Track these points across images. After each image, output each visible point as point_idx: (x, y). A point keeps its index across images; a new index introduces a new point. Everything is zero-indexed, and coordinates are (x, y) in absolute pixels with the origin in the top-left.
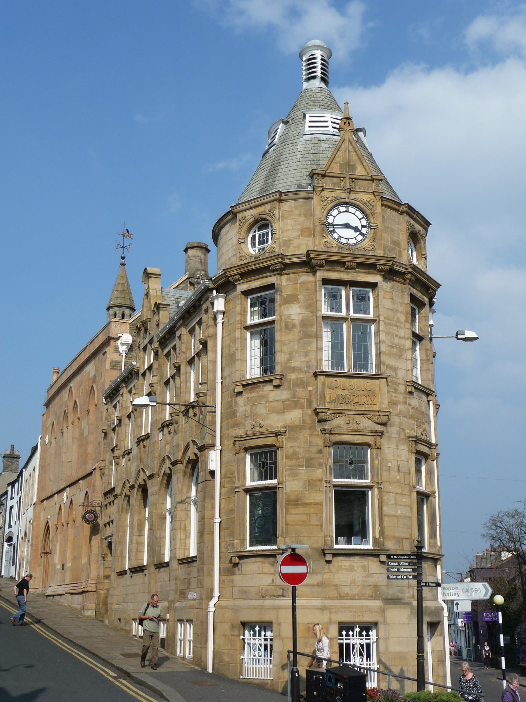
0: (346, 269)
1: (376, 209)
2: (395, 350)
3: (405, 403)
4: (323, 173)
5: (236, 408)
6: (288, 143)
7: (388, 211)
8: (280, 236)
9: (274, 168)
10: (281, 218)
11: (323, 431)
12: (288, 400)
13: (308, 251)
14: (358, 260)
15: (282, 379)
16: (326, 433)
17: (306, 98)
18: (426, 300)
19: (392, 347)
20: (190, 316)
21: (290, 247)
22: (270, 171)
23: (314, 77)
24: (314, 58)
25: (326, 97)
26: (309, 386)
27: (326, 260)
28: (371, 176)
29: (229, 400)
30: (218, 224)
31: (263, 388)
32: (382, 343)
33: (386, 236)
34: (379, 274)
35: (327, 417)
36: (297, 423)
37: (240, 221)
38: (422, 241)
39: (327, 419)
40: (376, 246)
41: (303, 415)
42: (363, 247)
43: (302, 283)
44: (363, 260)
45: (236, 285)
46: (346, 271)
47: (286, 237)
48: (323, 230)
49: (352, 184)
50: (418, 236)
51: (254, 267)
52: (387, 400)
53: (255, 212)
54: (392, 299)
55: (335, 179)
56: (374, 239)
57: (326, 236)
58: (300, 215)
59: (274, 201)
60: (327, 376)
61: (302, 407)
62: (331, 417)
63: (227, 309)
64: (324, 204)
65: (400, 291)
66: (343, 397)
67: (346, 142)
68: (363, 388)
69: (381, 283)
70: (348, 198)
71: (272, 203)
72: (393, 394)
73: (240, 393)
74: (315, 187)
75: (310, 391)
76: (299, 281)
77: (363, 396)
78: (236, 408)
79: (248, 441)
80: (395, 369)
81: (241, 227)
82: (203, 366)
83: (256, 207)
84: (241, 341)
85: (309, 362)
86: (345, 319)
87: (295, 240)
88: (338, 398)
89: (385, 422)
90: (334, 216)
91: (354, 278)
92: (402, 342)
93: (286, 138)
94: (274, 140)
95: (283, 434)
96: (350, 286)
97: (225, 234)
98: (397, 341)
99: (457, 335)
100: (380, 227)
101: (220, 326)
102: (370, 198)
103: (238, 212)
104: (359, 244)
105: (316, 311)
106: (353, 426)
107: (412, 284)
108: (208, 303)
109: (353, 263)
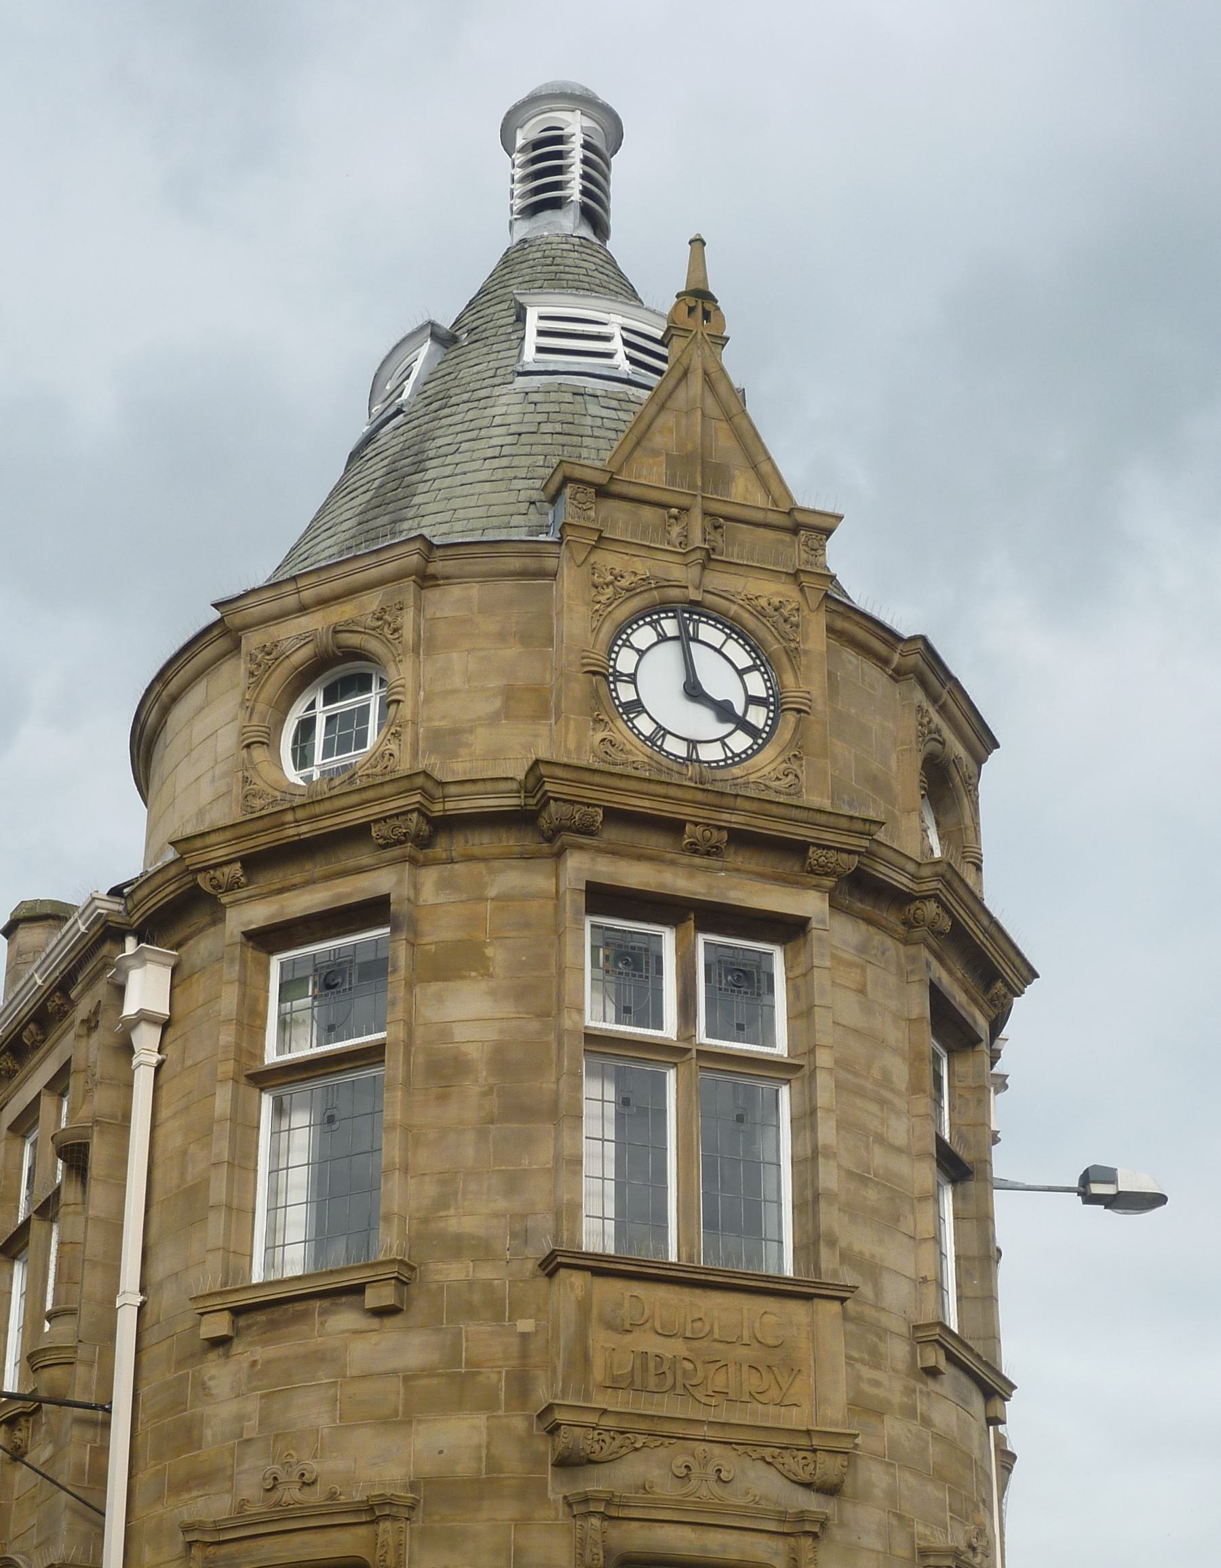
0: (683, 851)
1: (806, 638)
2: (872, 1195)
3: (910, 1412)
4: (602, 479)
5: (198, 1410)
6: (453, 400)
7: (850, 657)
8: (415, 714)
9: (398, 482)
10: (423, 646)
11: (580, 1506)
12: (428, 1372)
13: (537, 762)
14: (734, 818)
15: (405, 1284)
16: (591, 1514)
17: (524, 265)
18: (982, 1025)
19: (863, 1180)
20: (22, 1065)
21: (457, 756)
22: (382, 490)
23: (557, 204)
24: (559, 140)
25: (601, 269)
26: (522, 1317)
27: (606, 809)
28: (790, 513)
29: (169, 1377)
30: (158, 688)
31: (323, 1324)
32: (826, 1156)
33: (839, 747)
34: (816, 887)
35: (597, 1447)
36: (464, 1468)
37: (252, 658)
38: (966, 801)
39: (594, 1457)
40: (803, 777)
41: (489, 1435)
42: (752, 778)
43: (504, 899)
44: (754, 822)
45: (223, 907)
46: (685, 860)
47: (443, 718)
48: (595, 695)
49: (716, 536)
50: (952, 780)
51: (304, 829)
52: (843, 1387)
53: (316, 622)
54: (862, 991)
55: (648, 513)
56: (797, 752)
57: (607, 719)
58: (502, 637)
59: (397, 577)
60: (598, 1272)
61: (488, 1404)
62: (611, 1446)
63: (179, 1009)
64: (603, 599)
65: (893, 969)
66: (665, 1368)
67: (696, 383)
68: (746, 1333)
69: (822, 921)
70: (697, 588)
71: (390, 587)
72: (867, 1373)
73: (220, 1343)
74: (568, 530)
75: (524, 1336)
76: (492, 892)
77: (745, 1368)
78: (198, 1410)
79: (246, 1545)
80: (872, 1270)
81: (256, 678)
82: (67, 1248)
83: (324, 602)
84: (233, 1133)
85: (524, 1216)
86: (673, 1053)
87: (480, 730)
88: (645, 1369)
89: (835, 1480)
90: (638, 651)
91: (715, 891)
92: (901, 1165)
93: (446, 386)
94: (400, 395)
95: (404, 1513)
96: (702, 927)
97: (189, 722)
98: (879, 1158)
99: (1086, 1179)
100: (819, 705)
101: (143, 1081)
102: (783, 595)
103: (246, 627)
104: (734, 764)
105: (559, 1011)
106: (706, 1489)
107: (935, 945)
108: (101, 990)
109: (715, 832)
